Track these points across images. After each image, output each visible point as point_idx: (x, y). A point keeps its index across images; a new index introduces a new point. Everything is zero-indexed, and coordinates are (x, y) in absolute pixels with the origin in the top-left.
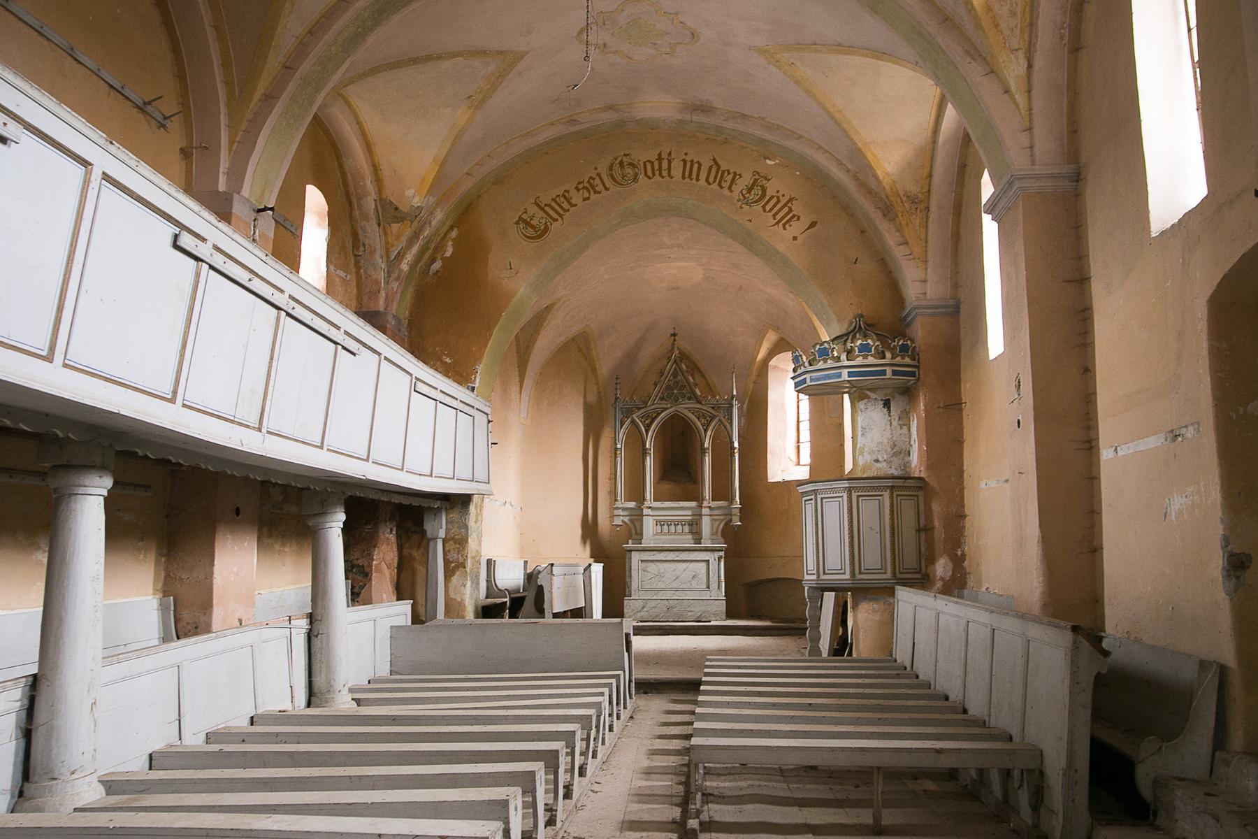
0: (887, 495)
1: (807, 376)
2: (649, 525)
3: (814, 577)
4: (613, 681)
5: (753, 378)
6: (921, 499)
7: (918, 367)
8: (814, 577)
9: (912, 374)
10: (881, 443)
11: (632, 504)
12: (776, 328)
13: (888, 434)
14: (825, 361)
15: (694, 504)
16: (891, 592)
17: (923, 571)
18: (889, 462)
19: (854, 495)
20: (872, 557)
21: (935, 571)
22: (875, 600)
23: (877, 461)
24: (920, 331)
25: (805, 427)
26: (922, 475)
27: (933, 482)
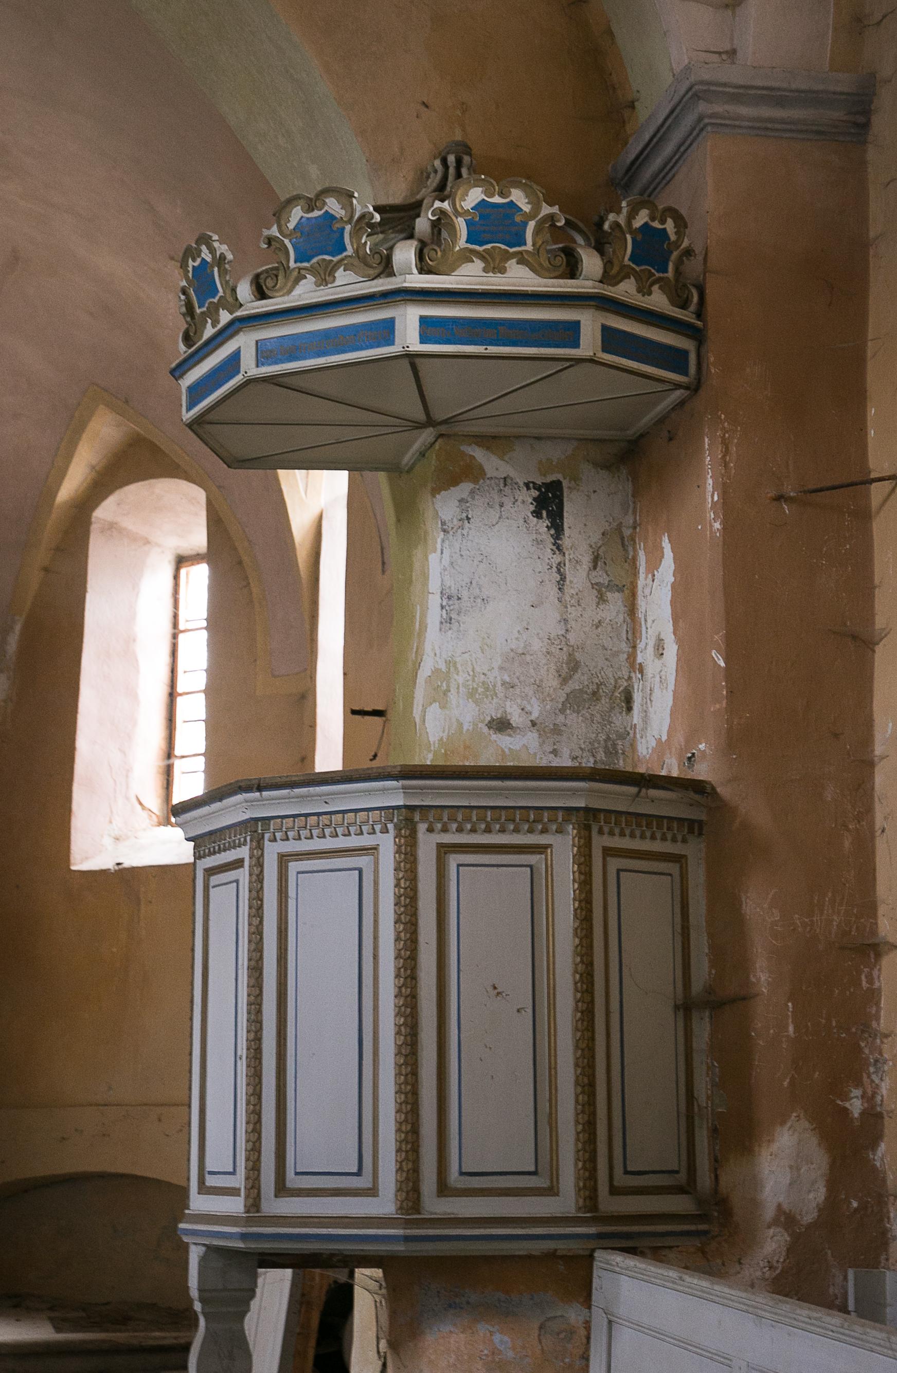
0: (563, 847)
1: (244, 343)
3: (235, 1206)
5: (41, 556)
6: (697, 876)
7: (697, 334)
8: (235, 1206)
9: (673, 359)
10: (518, 656)
12: (122, 403)
13: (548, 620)
14: (325, 275)
16: (573, 1277)
17: (704, 1180)
18: (550, 731)
19: (427, 844)
20: (499, 1117)
21: (755, 1183)
22: (501, 1312)
23: (502, 725)
24: (711, 195)
25: (193, 709)
26: (702, 772)
27: (754, 809)
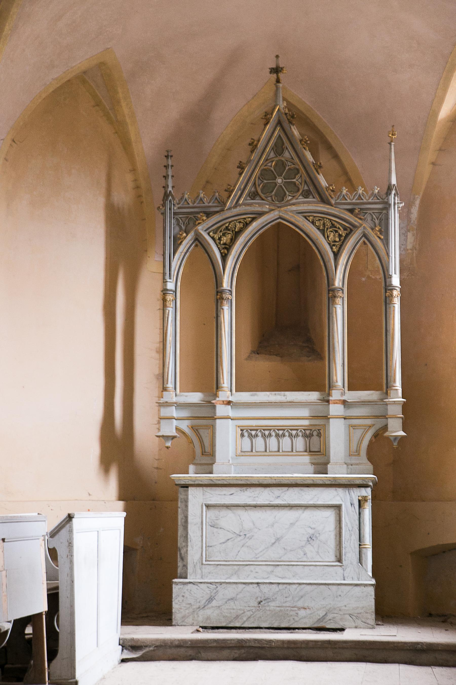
2: (227, 437)
11: (196, 397)
15: (314, 396)
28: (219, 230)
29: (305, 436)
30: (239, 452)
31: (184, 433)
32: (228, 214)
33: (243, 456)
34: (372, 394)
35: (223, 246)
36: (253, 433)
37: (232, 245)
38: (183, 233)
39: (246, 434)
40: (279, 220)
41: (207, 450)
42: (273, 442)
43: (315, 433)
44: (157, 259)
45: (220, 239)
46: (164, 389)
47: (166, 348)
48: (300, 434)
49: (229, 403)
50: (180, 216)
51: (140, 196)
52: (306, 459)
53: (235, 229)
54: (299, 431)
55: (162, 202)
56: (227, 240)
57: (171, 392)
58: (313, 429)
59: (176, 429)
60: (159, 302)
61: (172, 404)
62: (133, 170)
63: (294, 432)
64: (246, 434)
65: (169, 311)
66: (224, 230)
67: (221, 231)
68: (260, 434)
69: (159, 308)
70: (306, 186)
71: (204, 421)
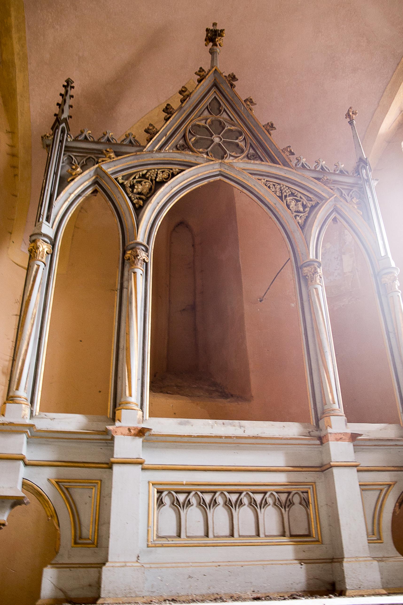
2: (131, 502)
4: (311, 487)
11: (72, 422)
15: (291, 429)
28: (133, 177)
29: (279, 505)
30: (153, 536)
31: (38, 494)
32: (148, 159)
33: (162, 546)
34: (385, 429)
35: (138, 196)
36: (182, 498)
37: (151, 196)
38: (77, 168)
39: (167, 500)
40: (218, 178)
41: (84, 534)
42: (245, 516)
43: (296, 499)
44: (23, 250)
45: (132, 187)
46: (10, 398)
47: (23, 326)
48: (270, 501)
49: (141, 432)
50: (75, 154)
51: (14, 167)
52: (287, 551)
53: (156, 178)
54: (268, 494)
55: (51, 132)
56: (143, 190)
57: (24, 406)
58: (294, 492)
59: (24, 484)
60: (10, 350)
61: (21, 428)
62: (12, 133)
63: (258, 498)
64: (167, 500)
65: (39, 266)
66: (139, 177)
67: (135, 178)
68: (194, 501)
69: (16, 313)
70: (251, 149)
71: (88, 468)
